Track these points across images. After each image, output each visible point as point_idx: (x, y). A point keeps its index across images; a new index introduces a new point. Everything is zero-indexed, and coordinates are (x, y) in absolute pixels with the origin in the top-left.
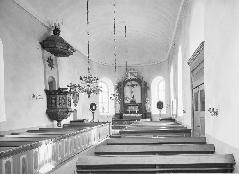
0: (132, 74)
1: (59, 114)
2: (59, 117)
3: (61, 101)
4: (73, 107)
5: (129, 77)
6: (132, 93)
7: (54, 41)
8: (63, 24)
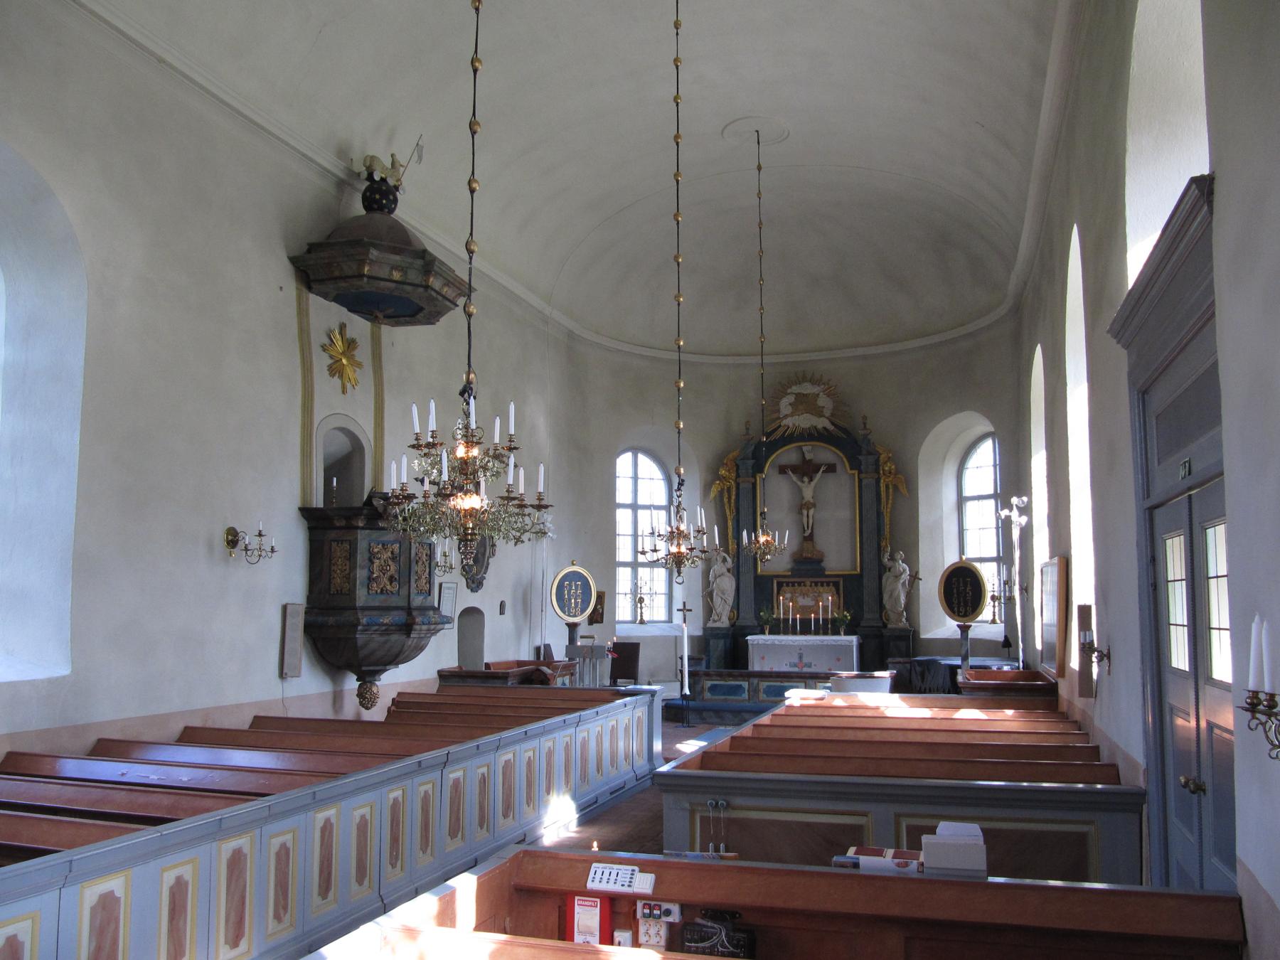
0: (805, 404)
1: (361, 638)
2: (362, 653)
3: (377, 562)
4: (453, 596)
5: (784, 422)
6: (805, 512)
7: (357, 243)
8: (420, 158)
